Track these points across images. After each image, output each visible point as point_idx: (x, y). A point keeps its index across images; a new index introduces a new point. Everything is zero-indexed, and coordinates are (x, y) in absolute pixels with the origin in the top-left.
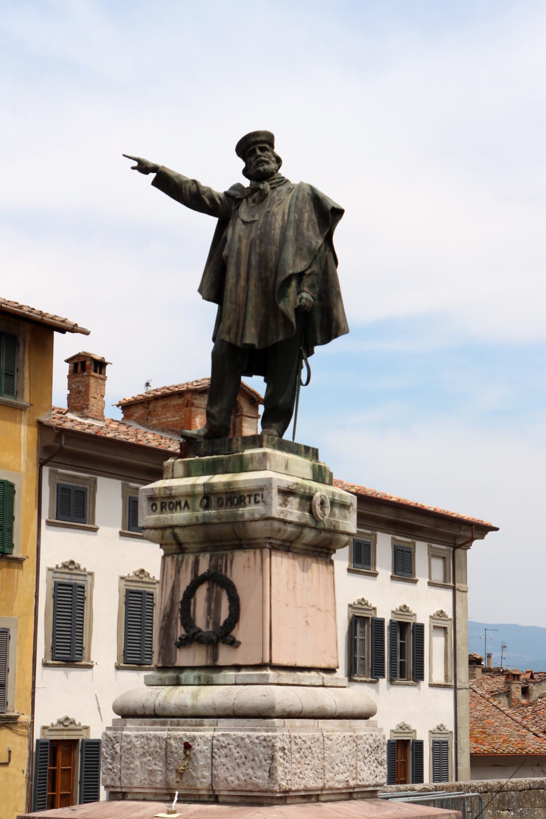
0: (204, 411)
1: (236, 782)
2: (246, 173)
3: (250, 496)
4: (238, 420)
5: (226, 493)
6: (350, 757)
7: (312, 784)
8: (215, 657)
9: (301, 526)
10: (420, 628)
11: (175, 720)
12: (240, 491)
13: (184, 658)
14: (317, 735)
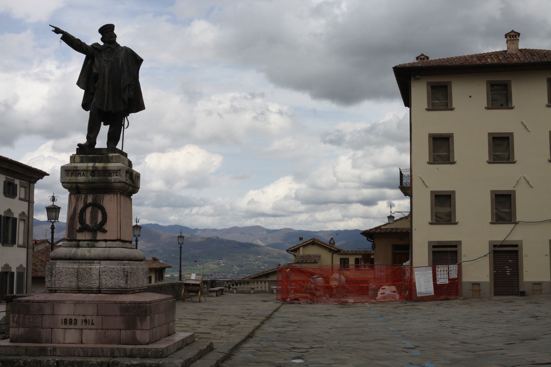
2: (102, 40)
8: (95, 235)
9: (130, 185)
10: (15, 219)
11: (81, 261)
12: (109, 170)
13: (80, 236)
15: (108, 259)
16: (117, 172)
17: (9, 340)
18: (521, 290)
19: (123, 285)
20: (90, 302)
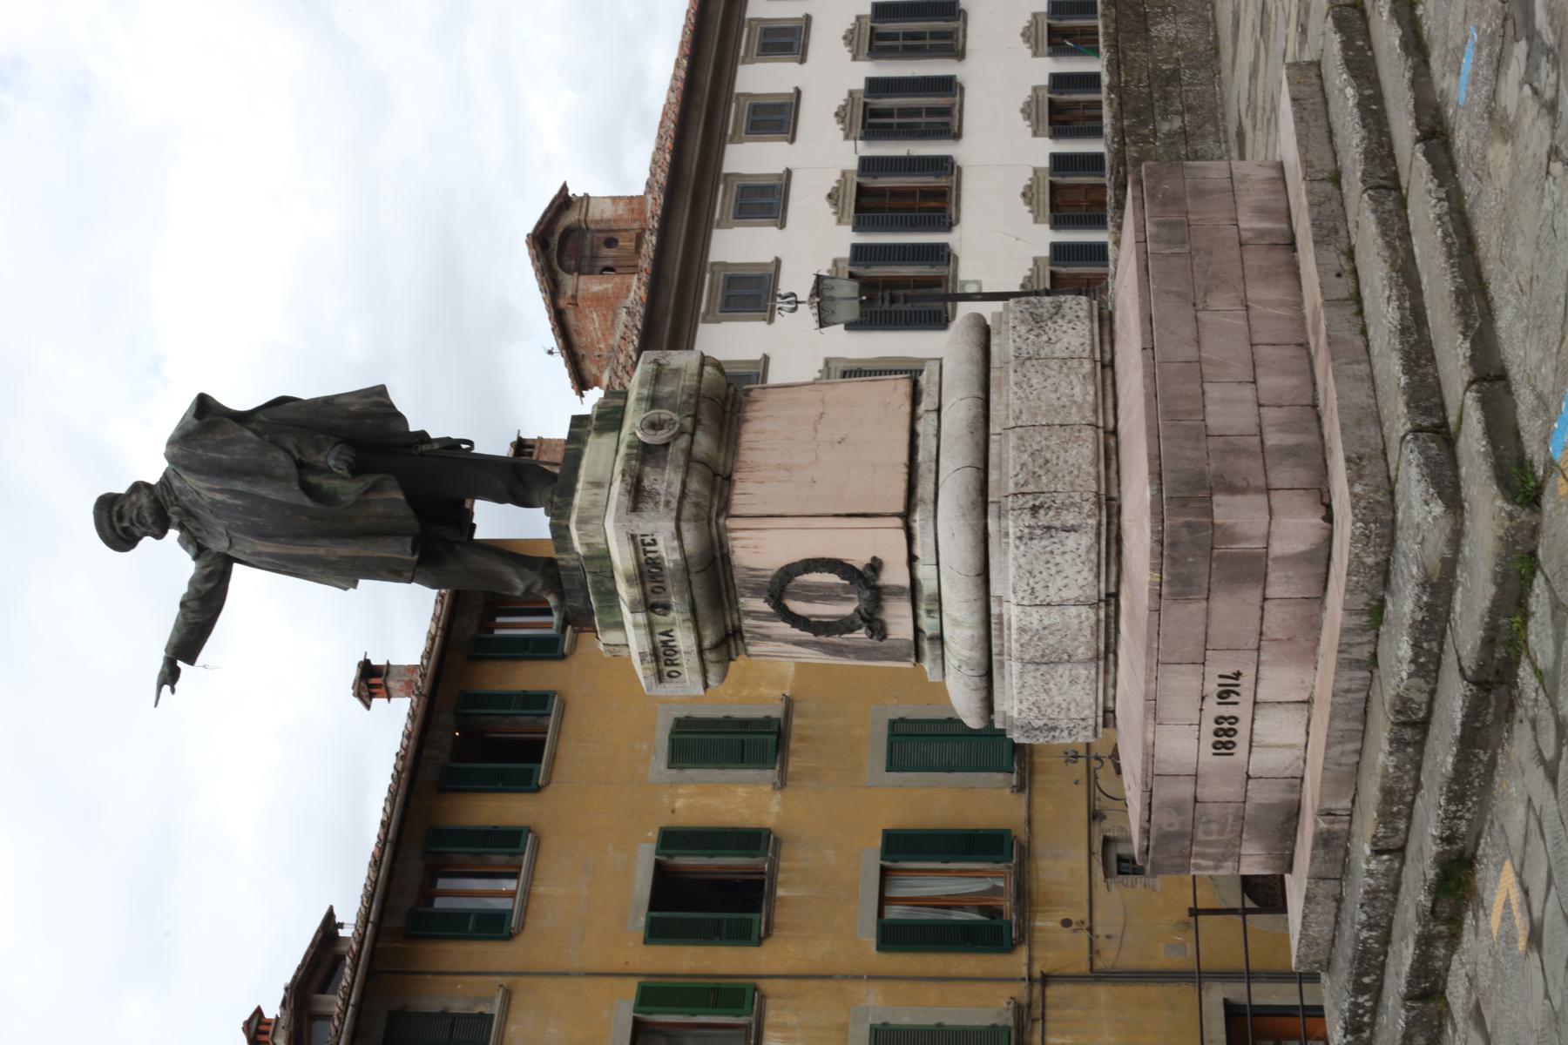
0: (583, 279)
1: (1085, 573)
2: (160, 535)
3: (645, 552)
4: (592, 226)
5: (643, 583)
6: (1048, 371)
7: (1088, 451)
8: (897, 592)
11: (995, 650)
12: (639, 565)
14: (1012, 438)
15: (984, 574)
16: (639, 544)
17: (1287, 876)
18: (1008, 1019)
19: (1087, 539)
20: (1153, 677)
